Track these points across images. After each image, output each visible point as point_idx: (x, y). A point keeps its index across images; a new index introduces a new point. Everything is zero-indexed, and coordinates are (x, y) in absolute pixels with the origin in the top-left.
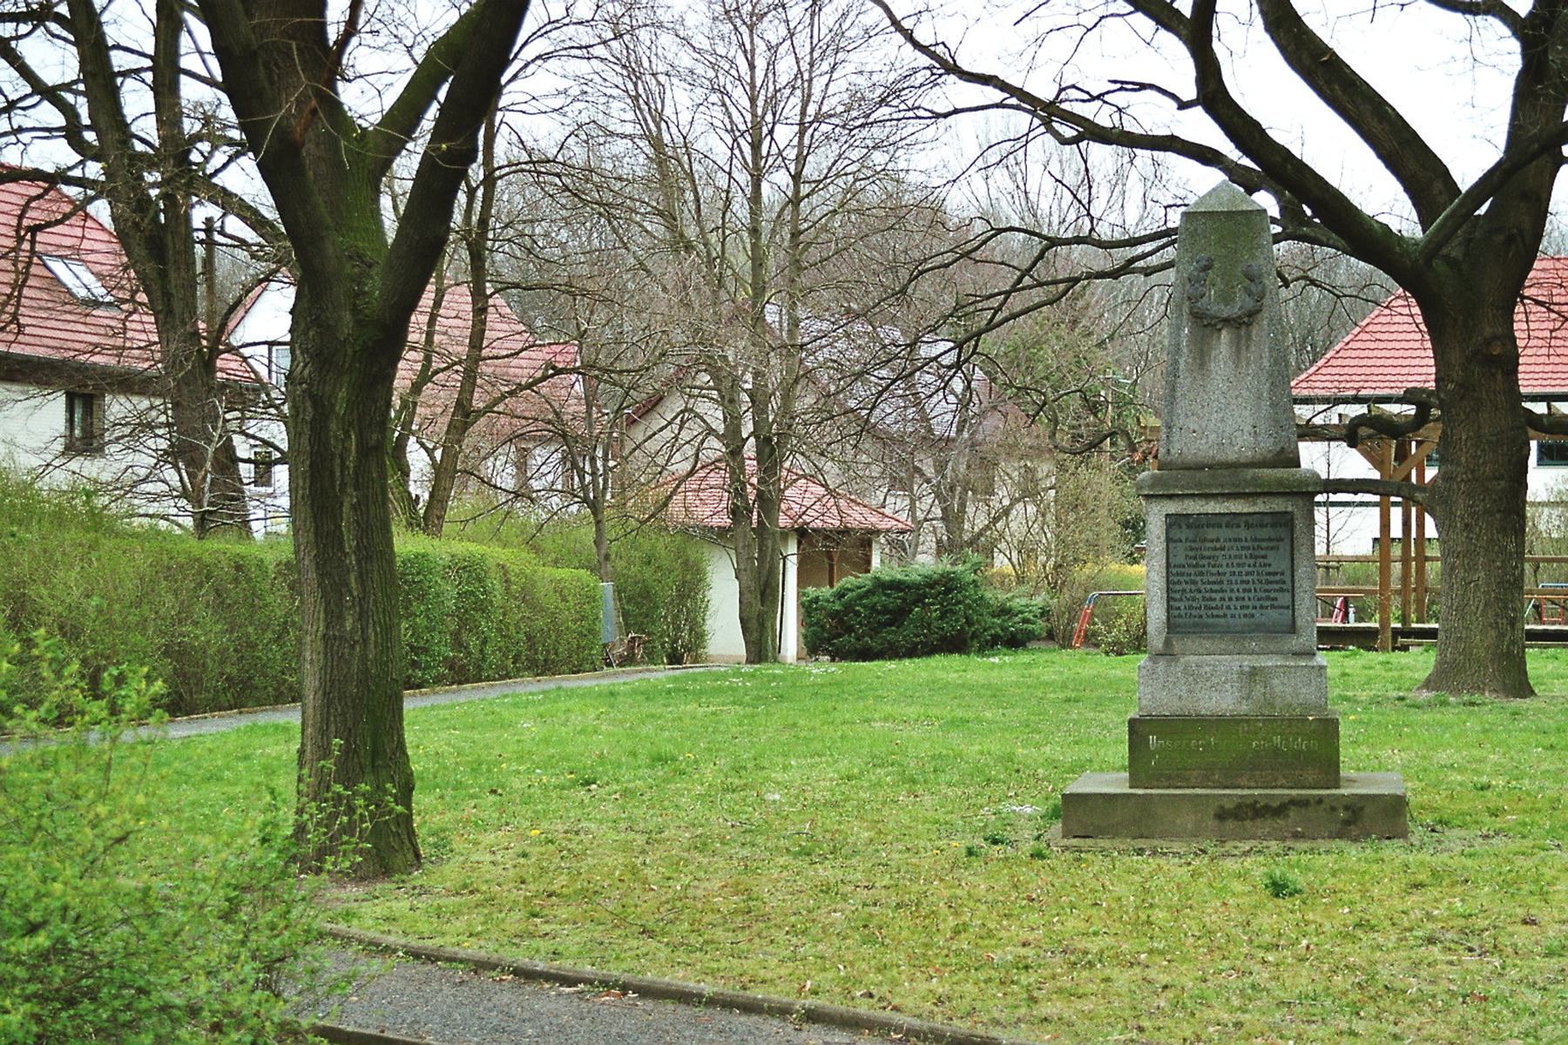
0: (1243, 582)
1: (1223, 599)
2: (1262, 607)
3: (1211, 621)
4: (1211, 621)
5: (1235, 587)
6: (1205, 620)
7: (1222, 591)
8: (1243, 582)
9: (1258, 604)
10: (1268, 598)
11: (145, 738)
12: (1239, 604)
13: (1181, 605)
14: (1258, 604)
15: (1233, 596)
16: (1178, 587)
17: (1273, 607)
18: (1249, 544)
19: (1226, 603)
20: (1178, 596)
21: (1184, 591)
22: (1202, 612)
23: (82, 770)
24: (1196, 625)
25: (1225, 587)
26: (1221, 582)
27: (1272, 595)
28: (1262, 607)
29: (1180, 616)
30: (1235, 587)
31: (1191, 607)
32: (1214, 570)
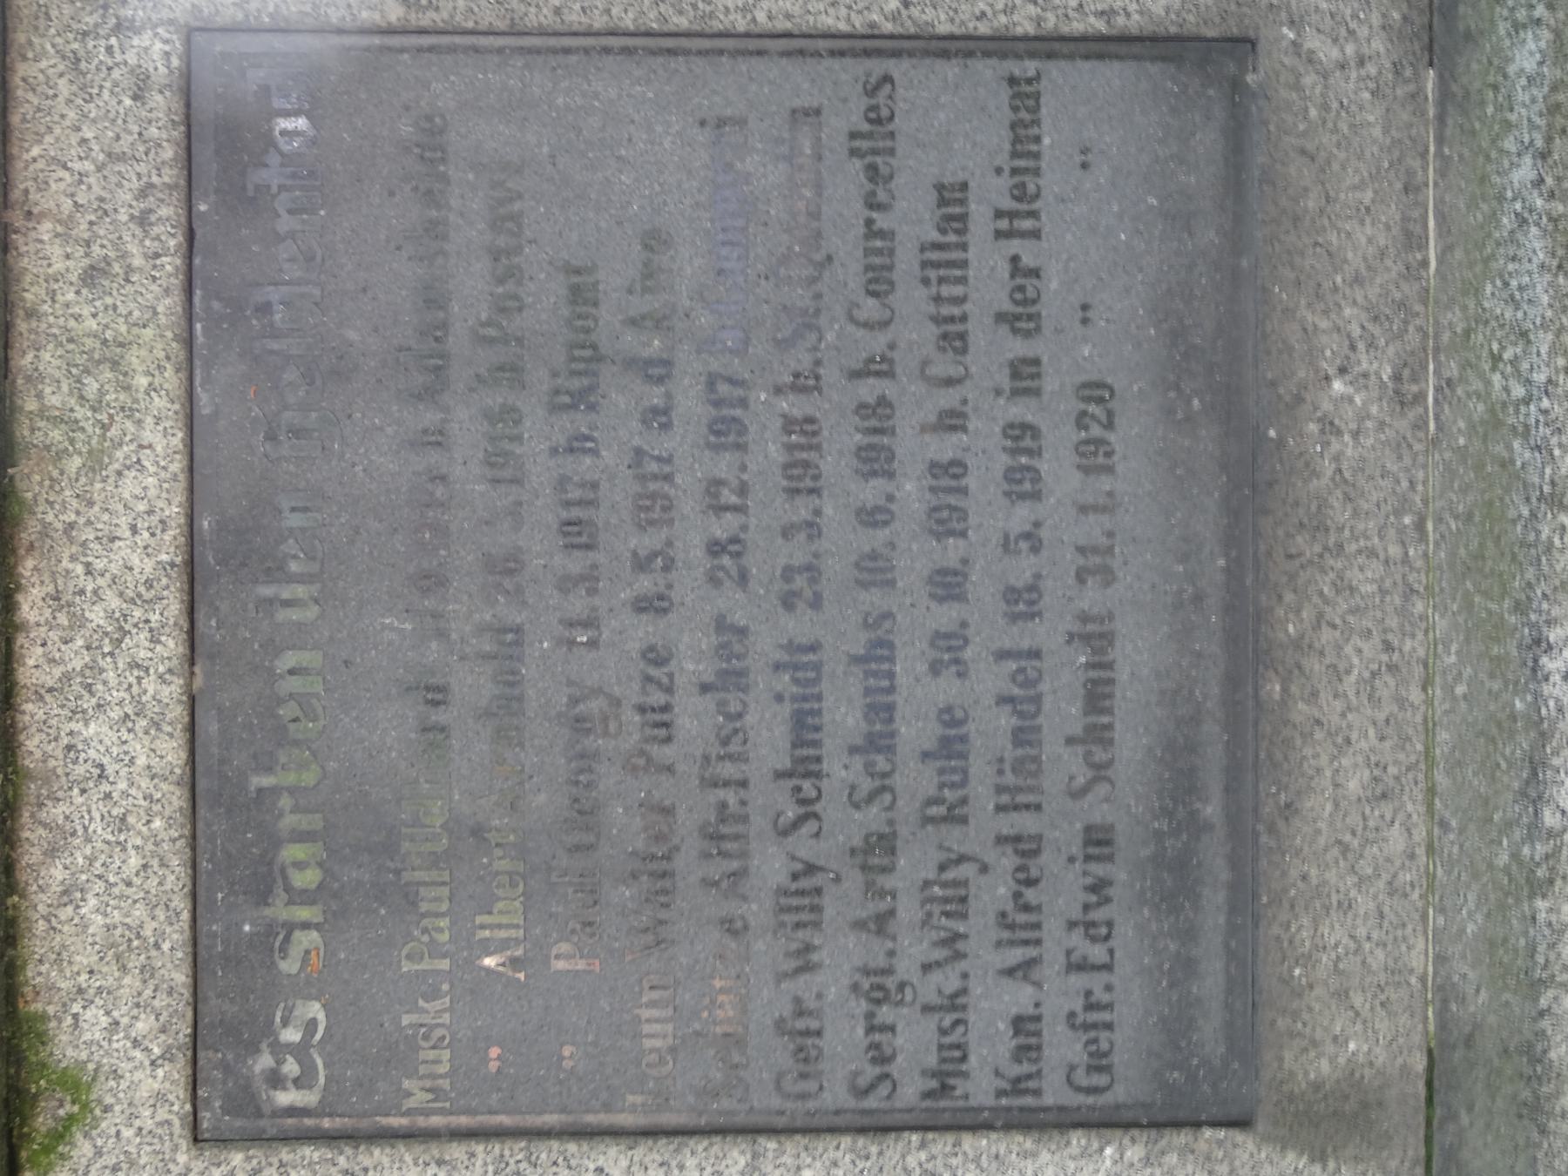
0: (801, 478)
1: (949, 650)
2: (1022, 316)
3: (1132, 743)
4: (1132, 743)
5: (843, 541)
6: (1126, 804)
7: (877, 654)
8: (801, 478)
9: (992, 350)
10: (945, 263)
11: (728, 764)
12: (990, 512)
13: (995, 1005)
14: (992, 350)
15: (916, 557)
16: (844, 1039)
17: (1018, 219)
18: (466, 422)
19: (987, 625)
20: (915, 1041)
21: (878, 988)
22: (1061, 832)
23: (1358, 683)
24: (1174, 881)
25: (838, 630)
26: (801, 660)
27: (913, 218)
28: (1022, 316)
29: (1092, 1019)
30: (843, 541)
31: (1020, 924)
32: (694, 719)
